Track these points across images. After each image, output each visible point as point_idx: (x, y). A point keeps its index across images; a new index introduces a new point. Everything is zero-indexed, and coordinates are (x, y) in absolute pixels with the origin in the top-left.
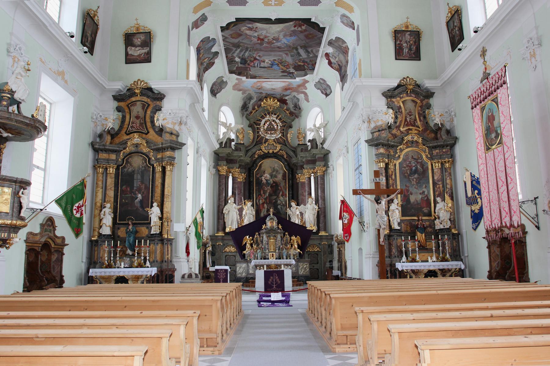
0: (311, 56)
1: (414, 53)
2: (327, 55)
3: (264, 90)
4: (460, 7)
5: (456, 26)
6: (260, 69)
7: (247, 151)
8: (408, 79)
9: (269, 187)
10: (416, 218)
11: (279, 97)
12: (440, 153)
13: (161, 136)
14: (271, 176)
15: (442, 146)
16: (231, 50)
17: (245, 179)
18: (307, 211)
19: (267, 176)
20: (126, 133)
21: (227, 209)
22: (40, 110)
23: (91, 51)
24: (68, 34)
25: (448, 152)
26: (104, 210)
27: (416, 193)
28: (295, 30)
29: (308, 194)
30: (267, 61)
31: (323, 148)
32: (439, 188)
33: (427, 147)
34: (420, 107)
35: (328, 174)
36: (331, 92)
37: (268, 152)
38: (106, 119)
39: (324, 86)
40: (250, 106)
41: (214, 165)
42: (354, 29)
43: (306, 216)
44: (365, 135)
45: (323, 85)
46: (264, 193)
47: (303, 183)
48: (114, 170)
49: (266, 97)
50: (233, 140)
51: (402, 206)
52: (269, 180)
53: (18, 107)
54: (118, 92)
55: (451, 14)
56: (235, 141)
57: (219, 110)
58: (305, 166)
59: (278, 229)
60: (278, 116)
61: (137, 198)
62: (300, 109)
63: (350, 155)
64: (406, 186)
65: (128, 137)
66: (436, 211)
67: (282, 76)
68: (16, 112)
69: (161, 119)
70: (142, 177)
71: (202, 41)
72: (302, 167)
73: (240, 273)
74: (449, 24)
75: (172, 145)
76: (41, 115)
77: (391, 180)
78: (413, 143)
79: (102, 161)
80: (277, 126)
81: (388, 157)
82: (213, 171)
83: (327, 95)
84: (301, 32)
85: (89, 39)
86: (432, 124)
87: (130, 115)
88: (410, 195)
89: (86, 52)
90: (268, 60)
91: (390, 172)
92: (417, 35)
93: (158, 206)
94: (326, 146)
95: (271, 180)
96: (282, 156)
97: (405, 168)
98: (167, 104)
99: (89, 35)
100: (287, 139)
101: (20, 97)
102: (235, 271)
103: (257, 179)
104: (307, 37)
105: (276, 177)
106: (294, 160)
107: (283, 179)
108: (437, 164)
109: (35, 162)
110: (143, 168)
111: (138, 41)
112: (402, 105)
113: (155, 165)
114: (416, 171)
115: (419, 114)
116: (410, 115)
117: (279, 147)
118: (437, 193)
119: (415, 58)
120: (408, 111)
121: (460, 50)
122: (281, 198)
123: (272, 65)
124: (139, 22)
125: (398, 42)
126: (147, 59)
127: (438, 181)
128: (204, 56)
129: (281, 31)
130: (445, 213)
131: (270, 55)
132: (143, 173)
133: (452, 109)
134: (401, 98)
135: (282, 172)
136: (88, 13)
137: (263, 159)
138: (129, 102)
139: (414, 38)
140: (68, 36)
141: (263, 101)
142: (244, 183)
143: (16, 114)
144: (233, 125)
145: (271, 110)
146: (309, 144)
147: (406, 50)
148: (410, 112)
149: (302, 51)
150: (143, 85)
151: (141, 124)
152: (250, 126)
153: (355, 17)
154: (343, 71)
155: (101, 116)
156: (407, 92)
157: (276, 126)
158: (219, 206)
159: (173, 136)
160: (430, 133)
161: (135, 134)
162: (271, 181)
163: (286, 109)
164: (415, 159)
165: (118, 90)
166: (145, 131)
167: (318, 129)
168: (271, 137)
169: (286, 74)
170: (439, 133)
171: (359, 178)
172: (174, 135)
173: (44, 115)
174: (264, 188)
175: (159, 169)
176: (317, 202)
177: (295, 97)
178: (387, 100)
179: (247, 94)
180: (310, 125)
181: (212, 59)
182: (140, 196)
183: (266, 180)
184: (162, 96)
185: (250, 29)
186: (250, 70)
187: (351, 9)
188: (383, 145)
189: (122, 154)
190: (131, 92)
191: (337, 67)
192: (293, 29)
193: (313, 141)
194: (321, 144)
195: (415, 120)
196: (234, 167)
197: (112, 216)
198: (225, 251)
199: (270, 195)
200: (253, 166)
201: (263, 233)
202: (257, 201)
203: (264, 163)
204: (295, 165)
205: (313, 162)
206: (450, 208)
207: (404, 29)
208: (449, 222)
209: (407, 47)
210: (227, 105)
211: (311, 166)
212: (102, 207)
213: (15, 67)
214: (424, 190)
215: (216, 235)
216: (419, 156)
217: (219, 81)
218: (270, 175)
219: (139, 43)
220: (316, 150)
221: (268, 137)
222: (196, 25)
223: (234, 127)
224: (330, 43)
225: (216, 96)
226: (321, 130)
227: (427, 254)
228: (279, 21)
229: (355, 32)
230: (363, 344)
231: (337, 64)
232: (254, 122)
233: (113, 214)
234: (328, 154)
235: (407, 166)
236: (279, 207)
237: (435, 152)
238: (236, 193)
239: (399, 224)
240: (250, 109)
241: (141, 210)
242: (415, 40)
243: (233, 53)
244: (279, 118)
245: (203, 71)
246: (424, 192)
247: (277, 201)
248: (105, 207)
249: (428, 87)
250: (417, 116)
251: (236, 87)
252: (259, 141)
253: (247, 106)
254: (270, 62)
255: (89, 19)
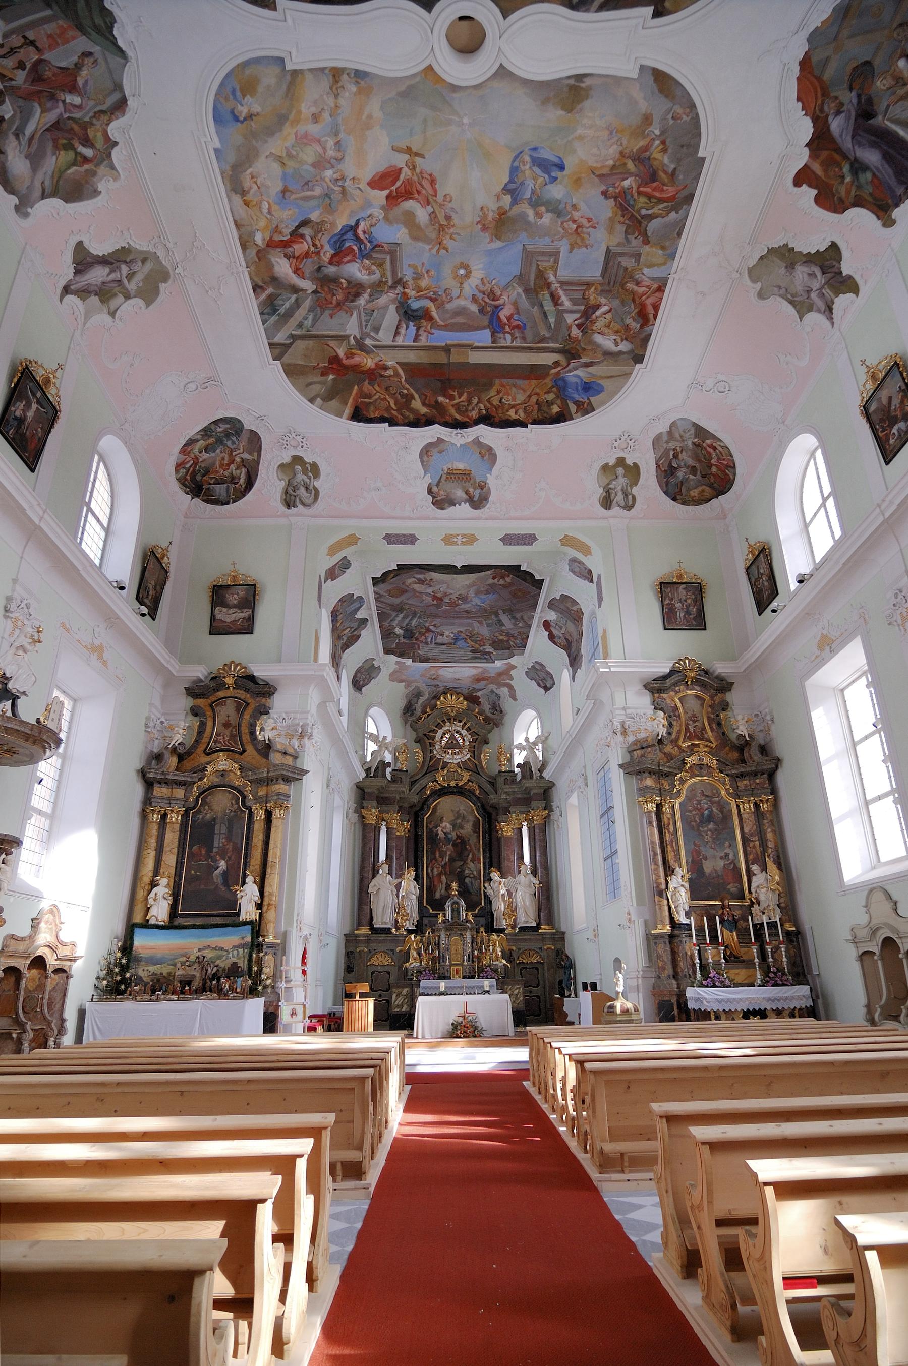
0: (520, 625)
1: (694, 619)
2: (547, 625)
3: (441, 681)
4: (768, 543)
5: (762, 574)
6: (435, 646)
7: (413, 783)
8: (687, 661)
9: (450, 846)
10: (718, 903)
11: (465, 692)
12: (750, 785)
13: (266, 756)
14: (454, 826)
15: (755, 774)
16: (389, 615)
17: (408, 831)
18: (519, 889)
19: (446, 825)
20: (205, 751)
21: (375, 885)
22: (52, 711)
23: (153, 614)
24: (115, 584)
25: (765, 784)
26: (155, 890)
27: (714, 857)
28: (494, 584)
29: (518, 859)
30: (447, 633)
31: (542, 777)
32: (754, 847)
33: (727, 775)
34: (710, 706)
35: (552, 825)
36: (554, 684)
37: (448, 785)
38: (171, 728)
39: (542, 674)
40: (419, 707)
41: (356, 807)
42: (592, 581)
43: (518, 900)
44: (617, 756)
45: (539, 673)
46: (442, 857)
47: (509, 838)
48: (180, 816)
49: (445, 693)
50: (389, 765)
51: (690, 881)
52: (450, 833)
53: (13, 705)
54: (195, 682)
55: (753, 555)
56: (392, 765)
57: (366, 714)
58: (512, 809)
59: (467, 922)
60: (465, 724)
61: (218, 867)
62: (501, 712)
63: (592, 791)
64: (694, 843)
65: (208, 759)
66: (753, 890)
67: (472, 657)
68: (9, 714)
69: (267, 729)
70: (230, 829)
71: (340, 600)
72: (507, 811)
73: (398, 1006)
74: (750, 571)
75: (284, 773)
76: (53, 720)
77: (667, 834)
78: (700, 768)
79: (159, 801)
80: (464, 740)
81: (661, 794)
82: (355, 817)
83: (546, 689)
84: (504, 586)
85: (151, 593)
86: (733, 737)
87: (214, 720)
88: (703, 861)
89: (143, 615)
90: (449, 632)
91: (665, 820)
92: (698, 590)
93: (255, 882)
94: (548, 774)
95: (454, 834)
96: (472, 792)
97: (690, 811)
98: (279, 704)
99: (151, 587)
100: (481, 763)
101: (17, 687)
102: (388, 1002)
103: (430, 831)
104: (514, 595)
105: (462, 827)
106: (493, 798)
107: (475, 832)
108: (747, 805)
109: (36, 802)
110: (232, 814)
111: (233, 598)
112: (679, 704)
113: (254, 807)
114: (710, 819)
115: (709, 718)
116: (694, 721)
117: (466, 776)
118: (751, 857)
119: (697, 626)
120: (689, 714)
121: (774, 611)
122: (471, 865)
123: (456, 639)
124: (237, 568)
125: (667, 602)
126: (247, 628)
127: (751, 835)
128: (343, 624)
129: (469, 586)
130: (770, 894)
131: (453, 624)
132: (231, 822)
133: (767, 710)
134: (677, 692)
135: (471, 819)
136: (152, 551)
137: (440, 796)
138: (214, 699)
139: (693, 594)
140: (115, 588)
141: (439, 699)
142: (408, 839)
143: (8, 717)
144: (389, 739)
145: (452, 714)
146: (516, 770)
147: (680, 614)
148: (694, 716)
149: (505, 618)
150: (239, 670)
151: (232, 736)
152: (418, 741)
153: (594, 563)
154: (573, 650)
155: (162, 723)
156: (687, 682)
157: (461, 741)
158: (361, 881)
159: (288, 757)
160: (730, 751)
161: (221, 754)
162: (453, 835)
163: (478, 713)
164: (707, 796)
165: (195, 678)
166: (239, 749)
167: (530, 747)
168: (454, 759)
169: (478, 655)
170: (746, 750)
171: (608, 829)
172: (290, 755)
173: (59, 720)
174: (442, 847)
175: (260, 815)
176: (534, 873)
177: (492, 692)
178: (654, 696)
179: (413, 688)
180: (519, 738)
181: (355, 630)
182: (223, 864)
183: (445, 833)
184: (272, 689)
185: (421, 582)
186: (419, 648)
187: (587, 550)
188: (651, 772)
189: (195, 789)
190: (217, 681)
191: (564, 643)
192: (491, 581)
193: (524, 766)
194: (539, 770)
195: (704, 729)
196: (390, 811)
197: (170, 902)
198: (372, 965)
199: (452, 860)
200: (422, 809)
201: (440, 930)
202: (430, 871)
203: (441, 803)
204: (494, 807)
205: (526, 801)
206: (778, 884)
207: (675, 580)
208: (778, 910)
209: (682, 609)
210: (380, 705)
211: (523, 809)
212: (153, 884)
213: (15, 637)
214: (728, 851)
215: (356, 932)
216: (715, 791)
217: (366, 667)
218: (451, 824)
219: (235, 602)
220: (531, 781)
221: (448, 758)
222: (332, 574)
223: (390, 743)
224: (552, 605)
225: (361, 690)
226: (537, 747)
227: (744, 970)
228: (469, 569)
229: (594, 586)
230: (672, 1189)
231: (563, 638)
232: (425, 735)
233: (171, 898)
234: (551, 787)
235: (695, 809)
236: (467, 880)
237: (743, 783)
238: (392, 857)
239: (688, 915)
240: (418, 712)
241: (224, 889)
242: (695, 598)
243: (391, 621)
244: (466, 727)
245: (342, 649)
246: (727, 855)
247: (464, 871)
248: (158, 885)
249: (723, 675)
250: (706, 723)
251: (395, 677)
252: (432, 766)
253: (413, 708)
254: (452, 636)
255: (153, 560)
